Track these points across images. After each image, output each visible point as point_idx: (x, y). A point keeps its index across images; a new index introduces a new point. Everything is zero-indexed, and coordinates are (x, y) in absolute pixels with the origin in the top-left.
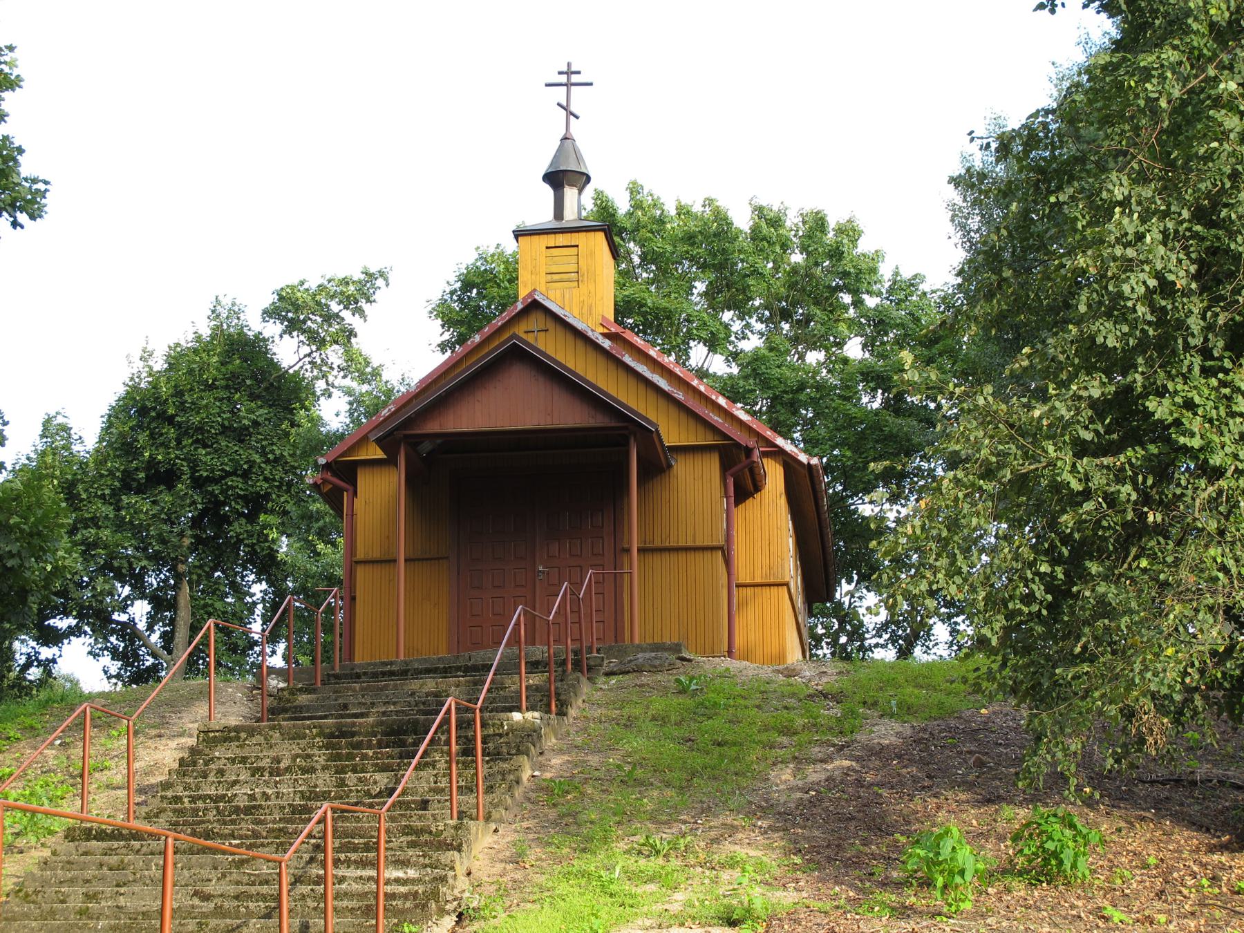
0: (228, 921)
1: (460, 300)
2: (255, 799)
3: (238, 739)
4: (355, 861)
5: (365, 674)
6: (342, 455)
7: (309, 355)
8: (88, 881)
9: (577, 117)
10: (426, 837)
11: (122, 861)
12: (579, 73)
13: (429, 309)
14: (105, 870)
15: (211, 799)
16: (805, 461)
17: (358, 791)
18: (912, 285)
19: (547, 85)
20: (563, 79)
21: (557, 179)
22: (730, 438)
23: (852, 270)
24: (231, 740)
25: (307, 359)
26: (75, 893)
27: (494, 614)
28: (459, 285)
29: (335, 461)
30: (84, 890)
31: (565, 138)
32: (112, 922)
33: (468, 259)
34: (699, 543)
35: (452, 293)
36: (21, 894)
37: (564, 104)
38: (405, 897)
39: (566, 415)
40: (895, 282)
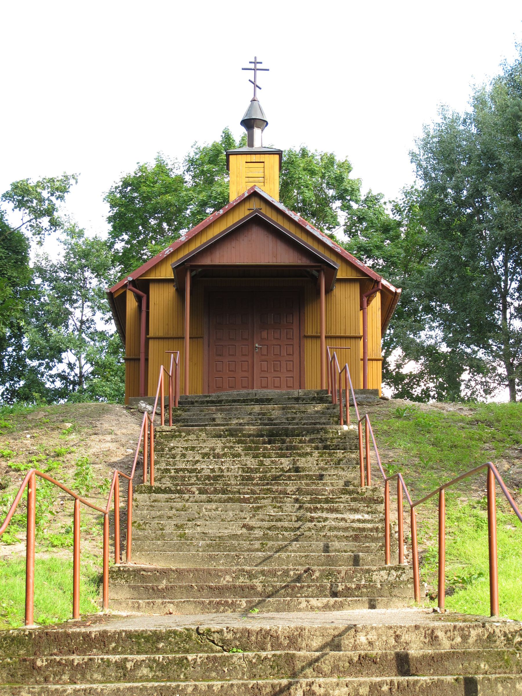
0: (280, 543)
1: (120, 192)
2: (214, 472)
3: (180, 436)
4: (326, 509)
5: (196, 401)
6: (141, 276)
7: (30, 221)
8: (170, 517)
9: (260, 88)
10: (355, 495)
11: (184, 506)
12: (261, 63)
13: (104, 196)
14: (174, 511)
15: (188, 471)
16: (394, 291)
17: (276, 468)
18: (376, 199)
19: (268, 70)
20: (252, 66)
21: (249, 123)
22: (366, 275)
23: (350, 189)
24: (176, 437)
25: (28, 224)
26: (170, 524)
27: (275, 371)
28: (121, 183)
29: (137, 279)
30: (175, 523)
31: (254, 100)
32: (208, 542)
33: (130, 170)
34: (348, 334)
35: (116, 188)
36: (135, 525)
37: (253, 81)
38: (371, 530)
39: (285, 257)
40: (368, 197)
